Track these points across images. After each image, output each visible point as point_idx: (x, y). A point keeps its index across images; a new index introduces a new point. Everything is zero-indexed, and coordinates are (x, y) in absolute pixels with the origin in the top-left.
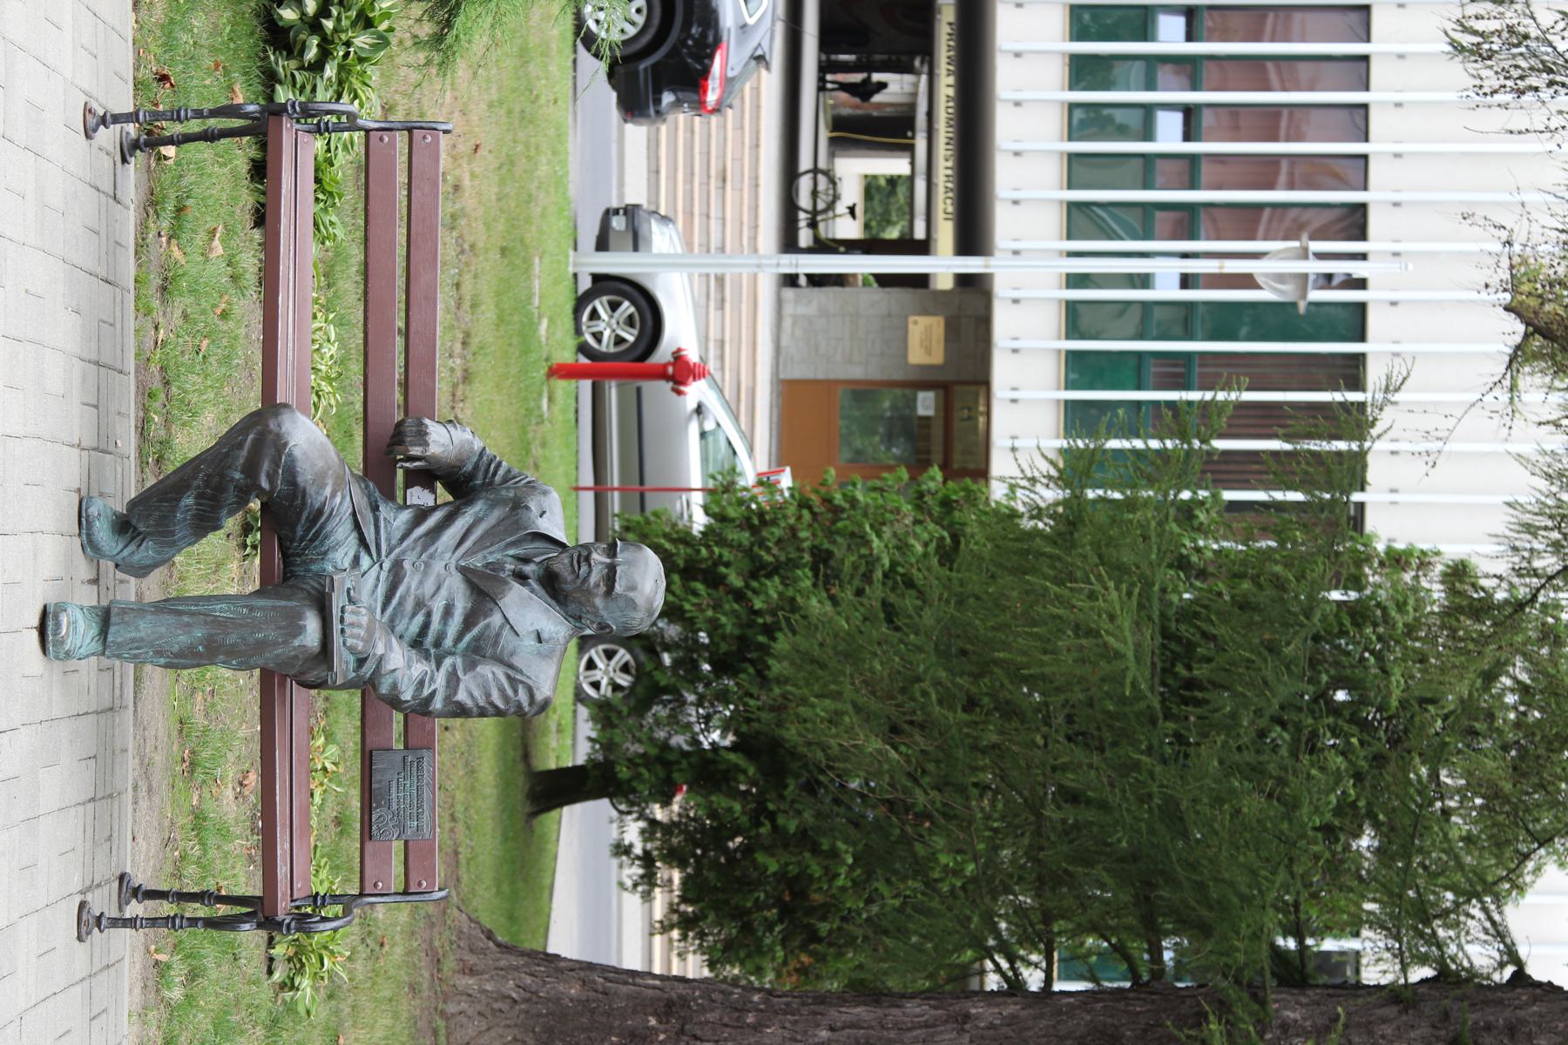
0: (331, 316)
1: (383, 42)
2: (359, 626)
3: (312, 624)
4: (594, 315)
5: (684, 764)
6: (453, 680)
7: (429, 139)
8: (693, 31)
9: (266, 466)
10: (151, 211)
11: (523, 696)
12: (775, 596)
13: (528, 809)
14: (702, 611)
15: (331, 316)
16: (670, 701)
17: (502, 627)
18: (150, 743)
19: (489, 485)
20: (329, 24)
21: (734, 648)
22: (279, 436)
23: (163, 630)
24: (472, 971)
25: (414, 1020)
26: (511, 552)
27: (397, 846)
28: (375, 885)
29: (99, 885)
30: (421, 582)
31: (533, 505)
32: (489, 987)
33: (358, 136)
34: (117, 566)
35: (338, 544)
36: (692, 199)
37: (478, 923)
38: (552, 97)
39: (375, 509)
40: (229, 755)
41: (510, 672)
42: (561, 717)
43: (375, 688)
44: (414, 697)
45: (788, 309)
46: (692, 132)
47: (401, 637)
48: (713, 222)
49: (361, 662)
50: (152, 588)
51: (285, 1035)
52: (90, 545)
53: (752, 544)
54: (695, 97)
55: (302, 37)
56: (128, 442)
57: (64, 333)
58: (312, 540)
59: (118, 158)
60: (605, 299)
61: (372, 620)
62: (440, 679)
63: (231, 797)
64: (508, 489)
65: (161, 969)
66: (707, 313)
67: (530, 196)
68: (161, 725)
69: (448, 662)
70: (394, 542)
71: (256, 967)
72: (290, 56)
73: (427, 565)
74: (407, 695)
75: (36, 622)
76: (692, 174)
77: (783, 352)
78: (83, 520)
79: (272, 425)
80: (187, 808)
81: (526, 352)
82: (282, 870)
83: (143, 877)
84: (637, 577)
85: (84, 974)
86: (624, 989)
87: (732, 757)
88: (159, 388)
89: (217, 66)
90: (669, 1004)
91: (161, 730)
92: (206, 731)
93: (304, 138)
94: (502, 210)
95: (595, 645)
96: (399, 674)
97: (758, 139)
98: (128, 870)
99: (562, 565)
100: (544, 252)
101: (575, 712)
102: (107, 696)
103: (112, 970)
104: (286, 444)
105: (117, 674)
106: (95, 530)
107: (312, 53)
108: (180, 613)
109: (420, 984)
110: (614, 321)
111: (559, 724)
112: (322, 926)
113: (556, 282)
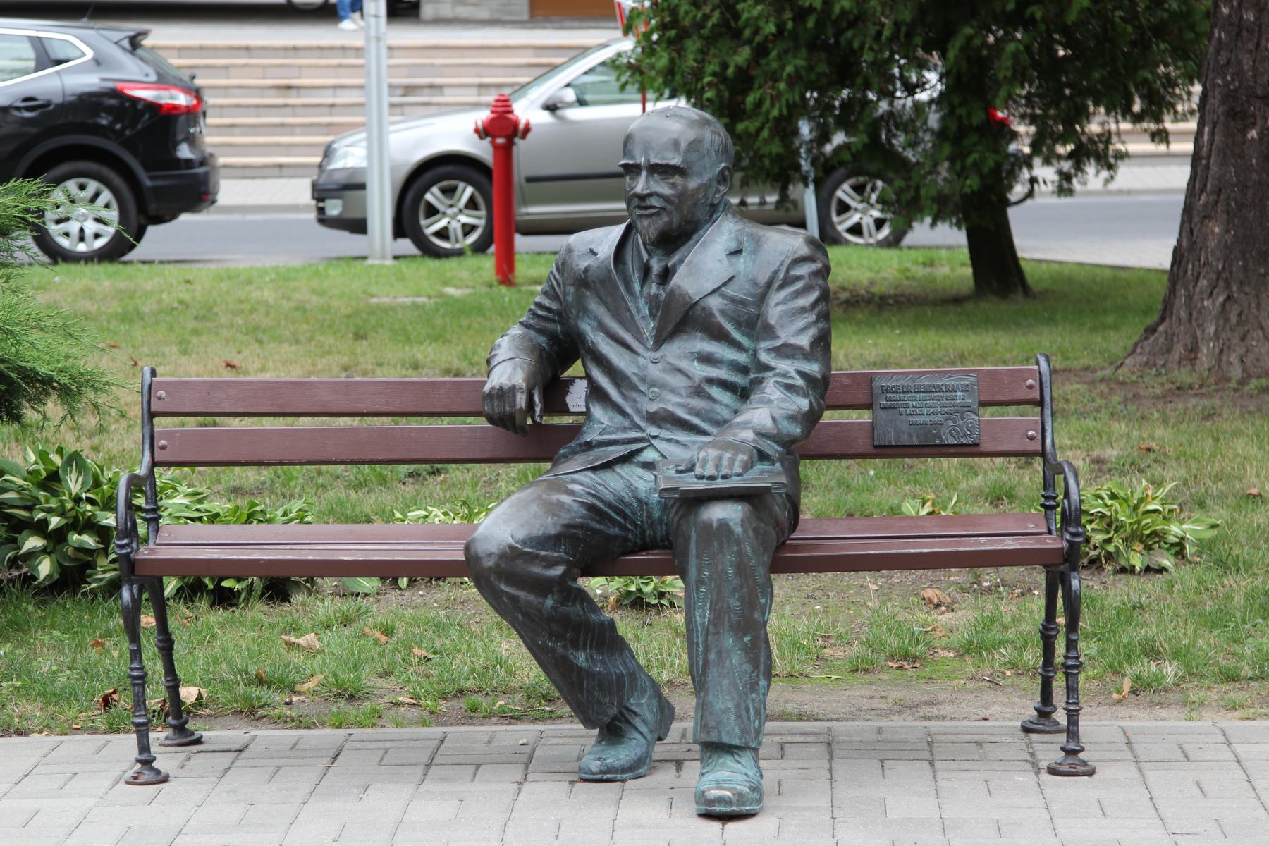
0: (398, 515)
1: (75, 460)
2: (720, 458)
3: (718, 512)
4: (443, 234)
5: (962, 111)
6: (786, 351)
7: (161, 393)
8: (104, 122)
9: (537, 570)
10: (261, 712)
11: (804, 270)
12: (759, 8)
13: (1020, 297)
14: (780, 94)
15: (398, 515)
16: (889, 131)
17: (724, 296)
18: (876, 703)
19: (561, 316)
20: (55, 521)
21: (823, 55)
22: (502, 556)
23: (725, 682)
24: (1193, 350)
25: (1246, 413)
26: (637, 287)
27: (987, 415)
28: (1032, 438)
29: (1032, 754)
30: (673, 391)
31: (583, 264)
32: (1211, 329)
33: (164, 476)
34: (660, 739)
35: (629, 487)
36: (311, 125)
37: (1136, 345)
38: (182, 287)
39: (589, 446)
40: (900, 618)
41: (776, 285)
42: (916, 263)
43: (794, 440)
44: (806, 396)
45: (446, 10)
46: (233, 126)
47: (736, 412)
48: (338, 100)
49: (763, 456)
50: (684, 702)
51: (1236, 552)
52: (635, 769)
53: (701, 37)
54: (183, 118)
55: (70, 552)
56: (524, 732)
57: (389, 802)
58: (625, 516)
59: (194, 748)
60: (423, 222)
61: (713, 445)
62: (786, 365)
63: (950, 615)
64: (565, 294)
65: (1140, 687)
66: (447, 104)
67: (297, 309)
68: (859, 692)
69: (764, 358)
70: (627, 424)
71: (1150, 588)
72: (92, 566)
73: (653, 384)
74: (803, 404)
75: (716, 825)
76: (282, 125)
77: (497, 16)
78: (606, 777)
79: (489, 563)
80: (957, 664)
81: (479, 310)
82: (1010, 544)
83: (1028, 708)
84: (665, 139)
85: (1133, 768)
86: (1214, 169)
87: (951, 54)
88: (464, 701)
89: (97, 644)
90: (1232, 114)
91: (863, 692)
92: (867, 643)
93: (164, 536)
94: (310, 339)
95: (832, 226)
96: (778, 413)
97: (239, 48)
98: (1019, 724)
99: (650, 227)
100: (365, 292)
101: (910, 248)
102: (814, 749)
103: (1133, 739)
104: (511, 547)
105: (789, 739)
106: (617, 764)
107: (89, 540)
108: (706, 662)
109: (1204, 408)
110: (450, 211)
111: (924, 264)
112: (1074, 496)
113: (402, 278)
